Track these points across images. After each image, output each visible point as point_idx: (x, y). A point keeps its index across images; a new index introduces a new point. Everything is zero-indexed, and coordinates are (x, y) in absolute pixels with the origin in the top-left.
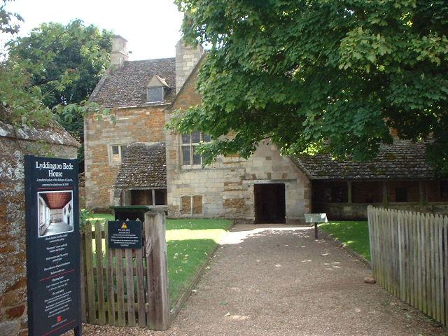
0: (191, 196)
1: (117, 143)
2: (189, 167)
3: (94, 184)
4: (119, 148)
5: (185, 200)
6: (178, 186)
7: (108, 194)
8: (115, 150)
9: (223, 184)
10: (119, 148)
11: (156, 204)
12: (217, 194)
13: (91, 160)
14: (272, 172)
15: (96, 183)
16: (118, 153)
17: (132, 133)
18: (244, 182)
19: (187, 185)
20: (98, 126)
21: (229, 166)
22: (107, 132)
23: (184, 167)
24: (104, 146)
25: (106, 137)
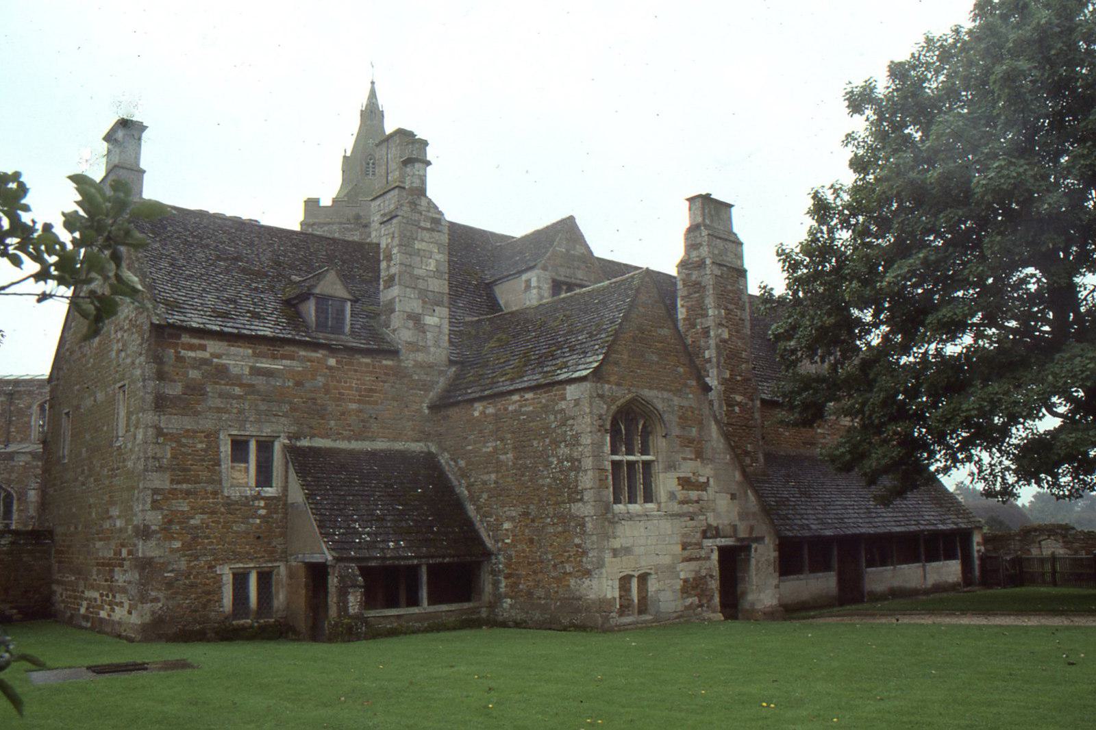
0: (636, 574)
1: (251, 430)
2: (635, 508)
3: (173, 551)
4: (253, 446)
5: (625, 581)
6: (615, 553)
7: (218, 579)
8: (239, 448)
9: (680, 547)
10: (253, 446)
11: (432, 601)
12: (671, 569)
13: (167, 476)
14: (738, 523)
15: (177, 544)
16: (246, 461)
17: (293, 409)
19: (627, 551)
20: (194, 374)
21: (685, 508)
23: (619, 508)
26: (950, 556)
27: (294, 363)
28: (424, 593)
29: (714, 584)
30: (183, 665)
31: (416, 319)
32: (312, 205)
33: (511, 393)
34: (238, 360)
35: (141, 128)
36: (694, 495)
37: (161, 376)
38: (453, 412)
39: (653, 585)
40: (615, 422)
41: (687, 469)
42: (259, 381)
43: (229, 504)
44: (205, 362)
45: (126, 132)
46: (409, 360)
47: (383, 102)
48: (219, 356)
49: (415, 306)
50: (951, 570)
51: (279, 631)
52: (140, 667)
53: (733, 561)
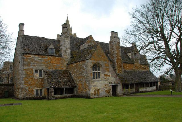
4: (39, 71)
5: (95, 91)
6: (93, 86)
7: (33, 91)
8: (37, 71)
10: (39, 71)
12: (103, 88)
15: (27, 85)
18: (110, 84)
19: (96, 86)
20: (29, 60)
22: (33, 63)
23: (94, 79)
24: (32, 69)
25: (33, 65)
26: (154, 86)
27: (45, 58)
28: (65, 93)
29: (111, 91)
30: (21, 104)
31: (65, 51)
32: (58, 35)
33: (78, 62)
34: (36, 58)
35: (23, 24)
36: (107, 77)
37: (24, 61)
38: (71, 65)
39: (100, 91)
40: (93, 66)
41: (106, 73)
42: (39, 61)
43: (35, 80)
44: (31, 58)
45: (21, 25)
46: (64, 57)
47: (69, 19)
48: (33, 58)
49: (65, 49)
50: (154, 88)
51: (43, 98)
52: (11, 104)
53: (114, 87)
